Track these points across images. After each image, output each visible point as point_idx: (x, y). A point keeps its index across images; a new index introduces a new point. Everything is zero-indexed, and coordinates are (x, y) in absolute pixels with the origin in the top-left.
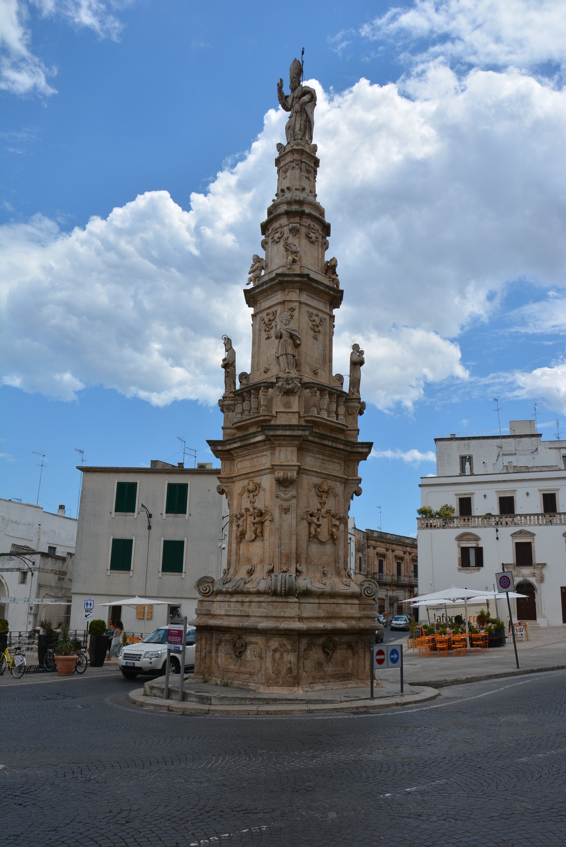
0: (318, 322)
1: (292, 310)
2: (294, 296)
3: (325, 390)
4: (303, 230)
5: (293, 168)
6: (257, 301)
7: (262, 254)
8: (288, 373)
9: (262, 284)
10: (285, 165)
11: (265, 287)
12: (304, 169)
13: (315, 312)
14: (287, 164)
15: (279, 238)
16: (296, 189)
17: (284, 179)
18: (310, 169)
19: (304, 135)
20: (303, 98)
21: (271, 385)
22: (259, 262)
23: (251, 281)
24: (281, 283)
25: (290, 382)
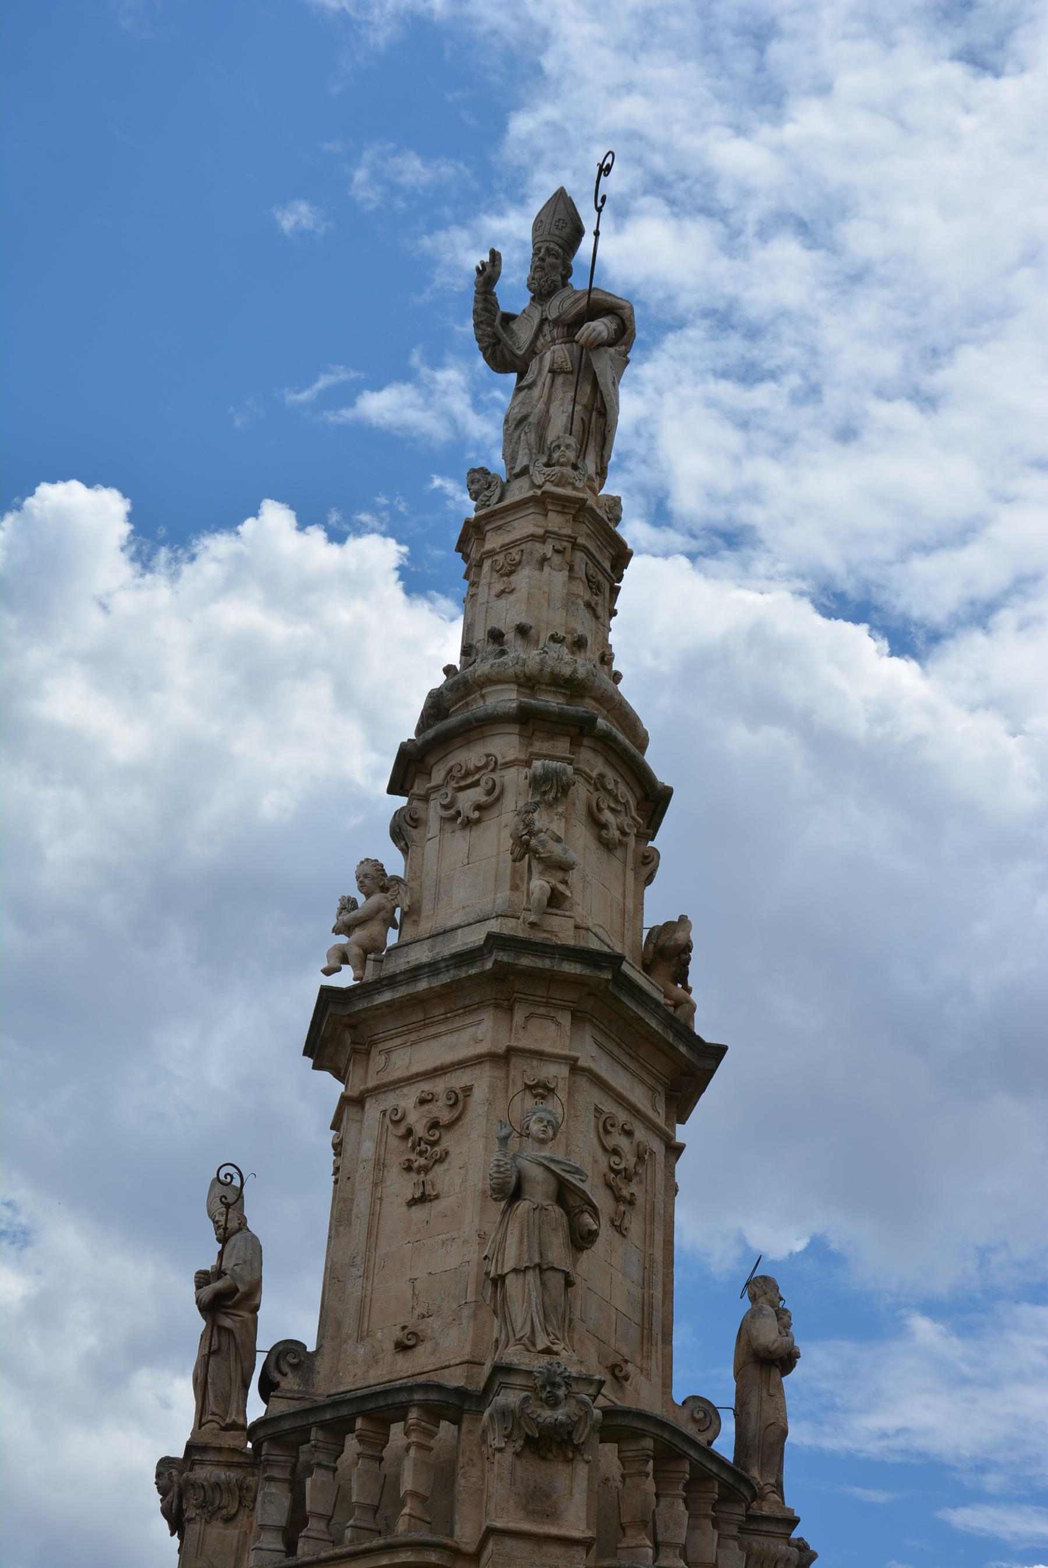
0: (629, 1160)
1: (542, 1090)
2: (552, 1035)
3: (682, 1456)
4: (581, 792)
5: (544, 560)
6: (374, 1043)
7: (394, 863)
8: (547, 1351)
9: (391, 981)
10: (506, 547)
11: (422, 985)
12: (580, 571)
13: (622, 1116)
14: (514, 543)
15: (479, 807)
16: (554, 638)
17: (498, 596)
18: (600, 577)
19: (582, 453)
20: (593, 324)
21: (454, 1400)
22: (384, 889)
23: (345, 960)
24: (501, 975)
25: (561, 1392)
